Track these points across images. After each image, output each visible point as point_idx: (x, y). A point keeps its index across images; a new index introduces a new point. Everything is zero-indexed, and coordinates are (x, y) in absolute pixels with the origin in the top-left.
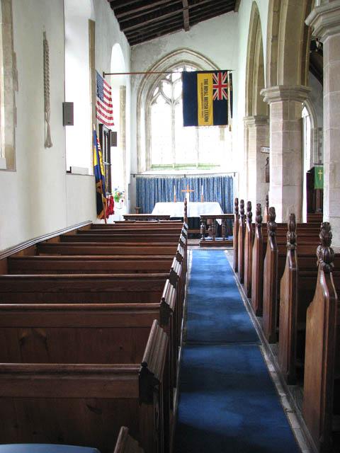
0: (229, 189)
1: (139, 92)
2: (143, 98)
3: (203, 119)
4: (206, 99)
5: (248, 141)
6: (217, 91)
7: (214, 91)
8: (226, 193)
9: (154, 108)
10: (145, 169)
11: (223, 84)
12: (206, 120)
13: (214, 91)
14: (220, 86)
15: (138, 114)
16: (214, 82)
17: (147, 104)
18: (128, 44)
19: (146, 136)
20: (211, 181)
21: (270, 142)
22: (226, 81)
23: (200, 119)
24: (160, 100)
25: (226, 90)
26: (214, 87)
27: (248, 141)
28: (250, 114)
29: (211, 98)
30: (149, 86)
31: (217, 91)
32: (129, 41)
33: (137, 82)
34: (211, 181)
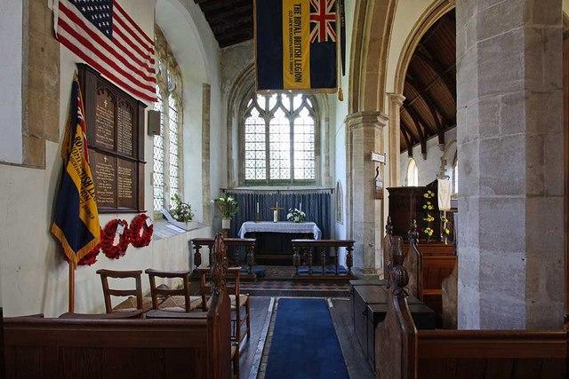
0: (327, 208)
1: (231, 101)
2: (236, 107)
3: (293, 77)
4: (298, 40)
5: (351, 147)
6: (318, 27)
7: (313, 26)
8: (324, 211)
9: (248, 121)
10: (237, 183)
11: (327, 13)
12: (299, 80)
13: (313, 26)
14: (322, 18)
15: (229, 124)
16: (313, 10)
17: (239, 114)
18: (213, 43)
19: (239, 149)
20: (307, 198)
21: (267, 223)
22: (333, 9)
23: (288, 78)
24: (255, 112)
25: (334, 25)
26: (312, 18)
27: (351, 147)
28: (355, 110)
29: (307, 38)
30: (242, 96)
31: (318, 27)
32: (217, 36)
33: (228, 89)
34: (307, 198)
